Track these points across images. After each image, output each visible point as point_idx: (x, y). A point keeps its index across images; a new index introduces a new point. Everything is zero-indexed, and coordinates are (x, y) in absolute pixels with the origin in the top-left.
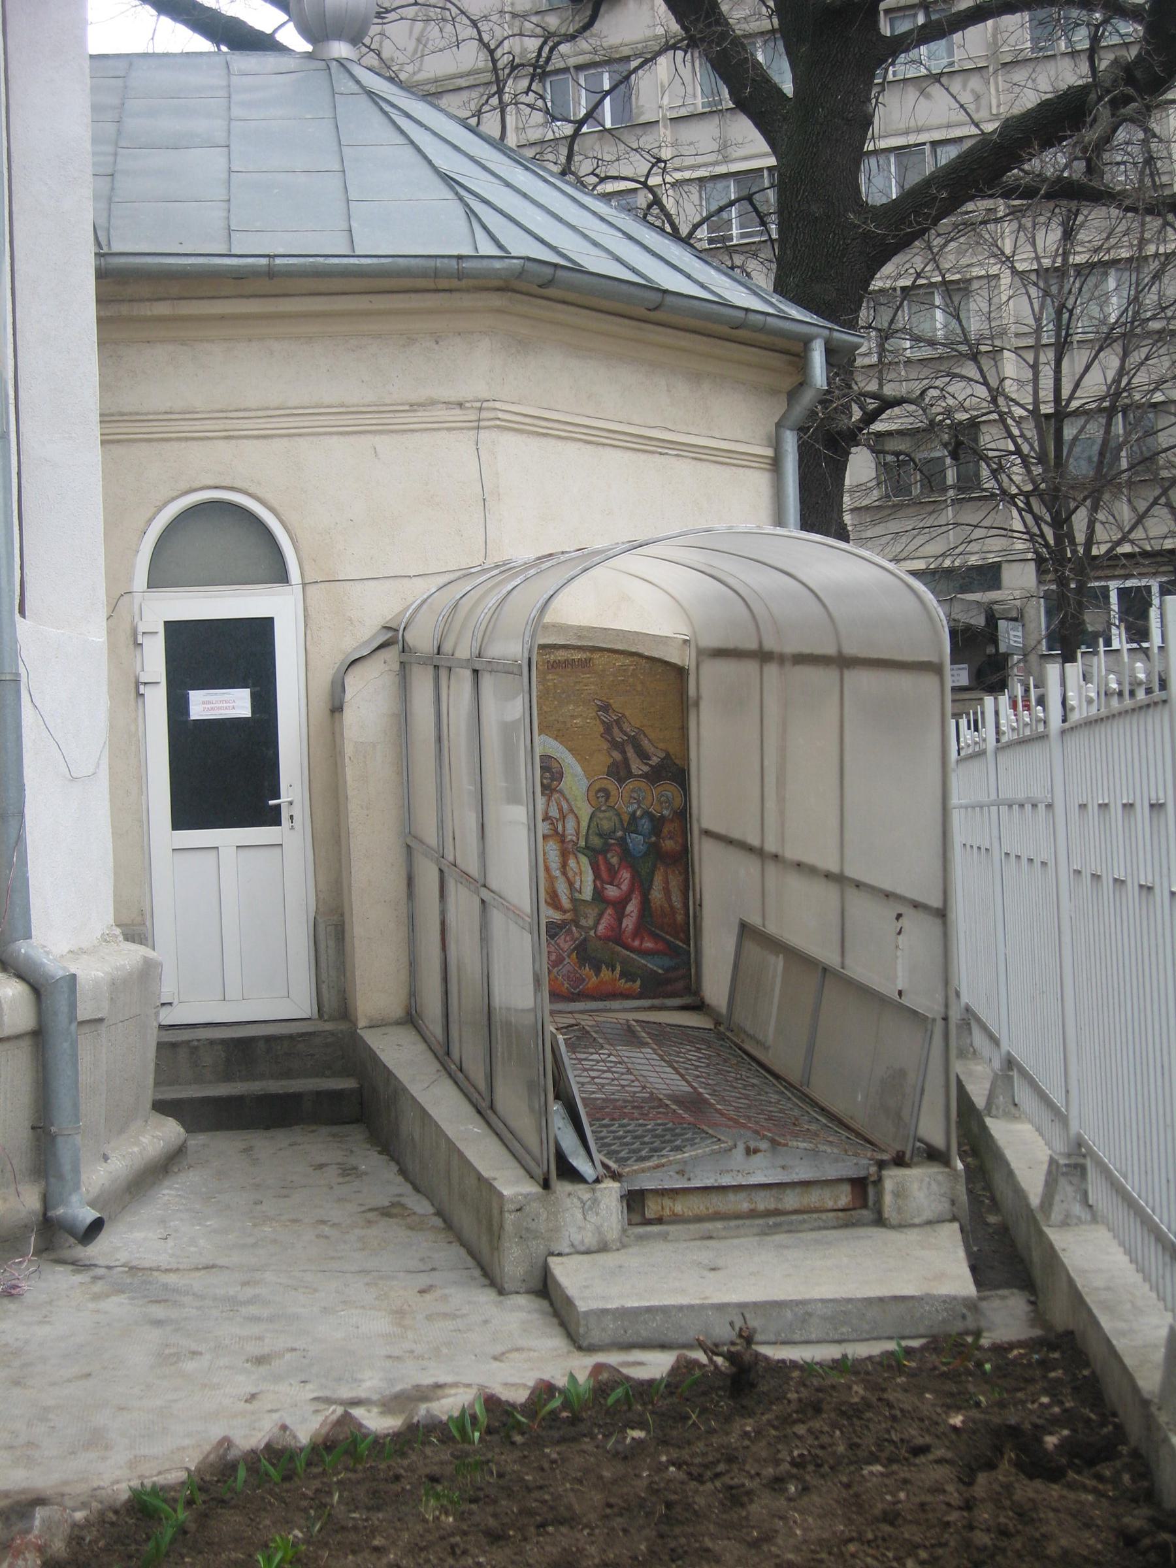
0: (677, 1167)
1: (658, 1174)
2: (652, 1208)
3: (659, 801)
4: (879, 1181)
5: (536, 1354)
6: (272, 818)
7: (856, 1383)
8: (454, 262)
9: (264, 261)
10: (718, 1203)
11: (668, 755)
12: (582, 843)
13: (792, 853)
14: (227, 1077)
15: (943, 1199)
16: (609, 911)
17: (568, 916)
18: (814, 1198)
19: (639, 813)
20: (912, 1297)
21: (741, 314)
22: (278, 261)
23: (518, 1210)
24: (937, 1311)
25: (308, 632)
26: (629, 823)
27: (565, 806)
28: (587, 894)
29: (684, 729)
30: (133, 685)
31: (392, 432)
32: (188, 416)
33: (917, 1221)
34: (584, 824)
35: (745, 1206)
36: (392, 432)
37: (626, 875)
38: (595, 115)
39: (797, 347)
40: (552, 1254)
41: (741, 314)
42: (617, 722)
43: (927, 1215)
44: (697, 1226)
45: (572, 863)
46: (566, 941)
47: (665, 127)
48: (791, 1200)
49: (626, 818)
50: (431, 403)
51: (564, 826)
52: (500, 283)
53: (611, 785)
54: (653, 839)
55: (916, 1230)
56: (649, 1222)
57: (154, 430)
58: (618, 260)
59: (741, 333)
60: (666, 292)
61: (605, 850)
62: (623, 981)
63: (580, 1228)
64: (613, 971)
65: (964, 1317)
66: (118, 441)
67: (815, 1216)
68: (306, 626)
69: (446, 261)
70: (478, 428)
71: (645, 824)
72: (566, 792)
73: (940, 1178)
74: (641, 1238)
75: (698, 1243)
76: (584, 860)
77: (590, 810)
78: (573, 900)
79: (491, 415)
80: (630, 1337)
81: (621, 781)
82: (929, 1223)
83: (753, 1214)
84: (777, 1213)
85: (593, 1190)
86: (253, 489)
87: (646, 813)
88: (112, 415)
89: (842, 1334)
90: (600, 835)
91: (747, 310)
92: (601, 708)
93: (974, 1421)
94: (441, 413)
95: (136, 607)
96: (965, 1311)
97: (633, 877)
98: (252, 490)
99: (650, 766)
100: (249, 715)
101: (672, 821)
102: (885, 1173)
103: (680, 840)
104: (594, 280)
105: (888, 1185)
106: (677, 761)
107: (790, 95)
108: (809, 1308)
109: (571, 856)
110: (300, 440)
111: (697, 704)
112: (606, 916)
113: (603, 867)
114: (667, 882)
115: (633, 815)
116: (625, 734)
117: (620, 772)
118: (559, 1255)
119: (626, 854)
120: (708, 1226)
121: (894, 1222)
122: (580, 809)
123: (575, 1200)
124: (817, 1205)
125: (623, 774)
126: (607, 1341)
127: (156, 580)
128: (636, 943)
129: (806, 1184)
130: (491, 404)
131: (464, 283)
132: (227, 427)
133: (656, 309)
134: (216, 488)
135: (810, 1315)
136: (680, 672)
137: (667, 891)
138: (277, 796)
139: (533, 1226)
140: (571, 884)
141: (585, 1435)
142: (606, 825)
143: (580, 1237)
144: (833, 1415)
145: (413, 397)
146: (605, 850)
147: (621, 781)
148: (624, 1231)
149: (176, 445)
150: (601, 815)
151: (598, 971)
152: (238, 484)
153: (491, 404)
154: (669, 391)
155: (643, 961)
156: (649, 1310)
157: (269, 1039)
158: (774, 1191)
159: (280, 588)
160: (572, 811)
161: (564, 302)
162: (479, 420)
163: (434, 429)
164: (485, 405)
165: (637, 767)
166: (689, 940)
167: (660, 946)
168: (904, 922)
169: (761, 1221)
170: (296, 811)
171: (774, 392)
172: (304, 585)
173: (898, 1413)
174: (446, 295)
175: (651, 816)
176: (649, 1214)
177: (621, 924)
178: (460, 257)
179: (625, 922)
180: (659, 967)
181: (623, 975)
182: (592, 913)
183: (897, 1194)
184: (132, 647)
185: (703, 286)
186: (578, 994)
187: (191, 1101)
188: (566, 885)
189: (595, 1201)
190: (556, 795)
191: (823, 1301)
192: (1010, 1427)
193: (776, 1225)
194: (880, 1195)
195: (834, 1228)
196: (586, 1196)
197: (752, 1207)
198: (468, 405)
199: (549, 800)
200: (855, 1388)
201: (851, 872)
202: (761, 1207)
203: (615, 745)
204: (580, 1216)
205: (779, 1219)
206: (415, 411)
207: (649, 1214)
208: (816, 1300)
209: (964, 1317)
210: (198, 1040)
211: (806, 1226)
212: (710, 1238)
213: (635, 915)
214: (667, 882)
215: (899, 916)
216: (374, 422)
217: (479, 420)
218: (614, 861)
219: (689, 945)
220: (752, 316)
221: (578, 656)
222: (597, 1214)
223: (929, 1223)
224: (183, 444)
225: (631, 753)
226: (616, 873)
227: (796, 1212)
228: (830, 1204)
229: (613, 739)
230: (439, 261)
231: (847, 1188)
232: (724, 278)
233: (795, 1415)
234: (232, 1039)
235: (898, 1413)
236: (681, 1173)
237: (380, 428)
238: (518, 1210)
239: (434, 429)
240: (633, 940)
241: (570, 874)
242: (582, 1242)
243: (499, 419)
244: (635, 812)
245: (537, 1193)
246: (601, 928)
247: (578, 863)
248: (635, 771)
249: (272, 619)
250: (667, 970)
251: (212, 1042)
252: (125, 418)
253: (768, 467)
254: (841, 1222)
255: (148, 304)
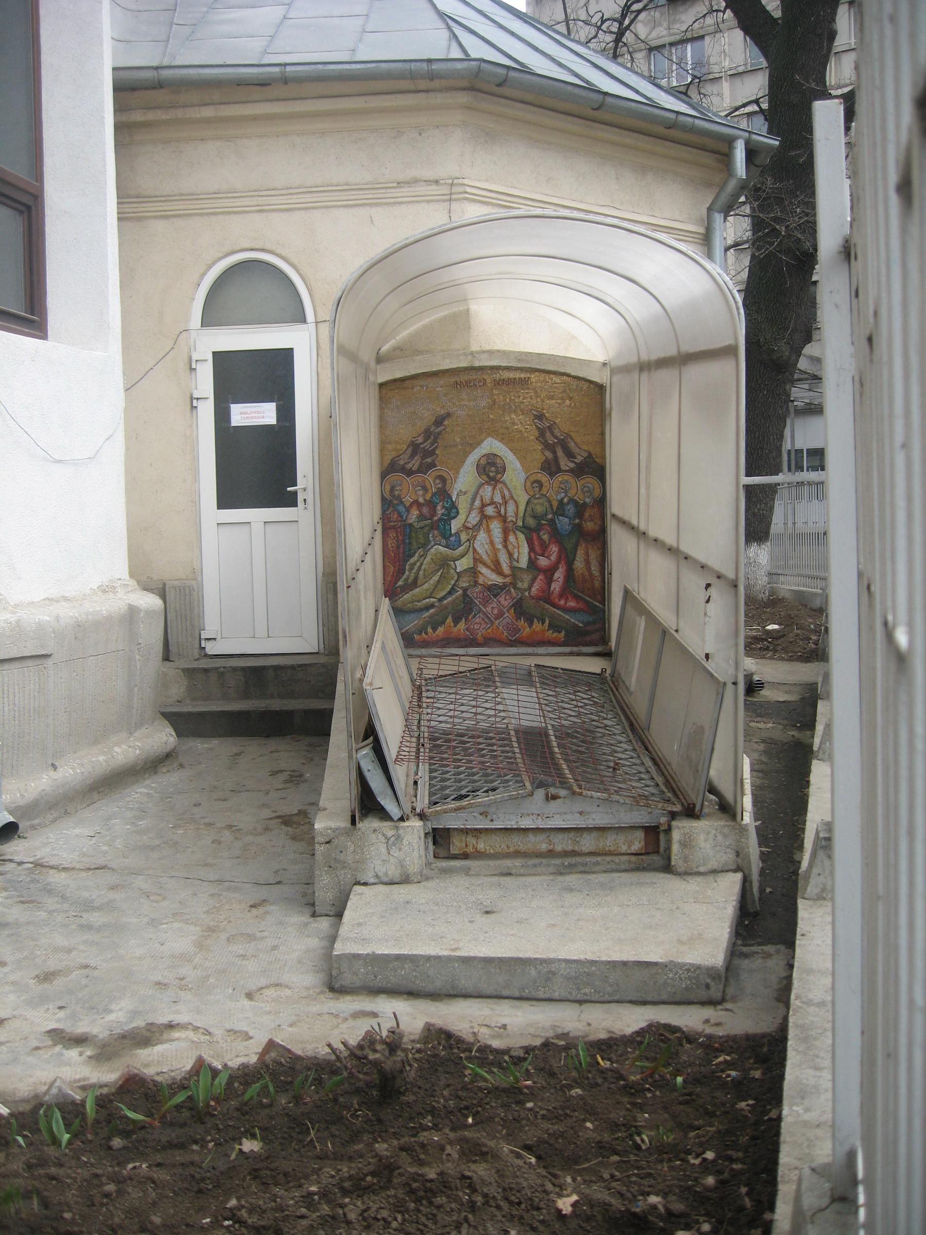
0: (482, 809)
1: (462, 814)
2: (457, 845)
3: (582, 491)
4: (669, 830)
5: (288, 992)
6: (291, 501)
7: (451, 1143)
8: (425, 65)
9: (277, 69)
10: (517, 843)
11: (590, 455)
12: (520, 523)
13: (653, 532)
14: (246, 695)
15: (728, 850)
16: (541, 577)
17: (508, 580)
18: (610, 842)
19: (566, 500)
20: (656, 964)
21: (673, 116)
22: (288, 69)
23: (327, 843)
24: (681, 979)
25: (319, 359)
26: (558, 508)
27: (507, 494)
28: (524, 562)
29: (603, 434)
30: (189, 400)
31: (385, 204)
32: (229, 195)
33: (702, 869)
34: (522, 508)
35: (544, 847)
36: (385, 204)
37: (554, 549)
38: (631, 28)
39: (723, 148)
40: (358, 883)
41: (673, 116)
42: (550, 428)
43: (713, 864)
44: (498, 862)
45: (512, 538)
46: (506, 600)
47: (726, 80)
48: (587, 843)
49: (555, 504)
50: (415, 181)
51: (505, 510)
52: (464, 83)
53: (544, 478)
54: (577, 521)
55: (699, 879)
56: (455, 857)
57: (203, 206)
58: (560, 65)
59: (673, 133)
60: (606, 94)
61: (538, 529)
62: (551, 632)
63: (384, 861)
64: (543, 623)
65: (707, 986)
66: (179, 216)
67: (608, 858)
68: (318, 355)
69: (418, 64)
70: (450, 200)
71: (571, 509)
72: (508, 482)
73: (726, 830)
74: (444, 871)
75: (495, 879)
76: (521, 537)
77: (527, 497)
78: (512, 568)
79: (461, 189)
80: (379, 982)
81: (552, 475)
82: (714, 872)
83: (551, 854)
84: (574, 853)
85: (397, 828)
86: (279, 250)
87: (572, 500)
88: (175, 195)
89: (585, 994)
90: (534, 517)
91: (678, 113)
92: (536, 417)
93: (591, 1204)
94: (422, 189)
95: (192, 340)
96: (708, 981)
97: (560, 551)
98: (279, 251)
99: (575, 463)
100: (275, 423)
101: (593, 506)
102: (674, 823)
103: (599, 522)
104: (544, 81)
105: (676, 835)
106: (597, 460)
107: (778, 14)
108: (554, 967)
109: (511, 533)
110: (315, 211)
111: (610, 414)
112: (538, 581)
113: (536, 543)
114: (587, 554)
115: (561, 502)
116: (556, 438)
117: (551, 468)
118: (365, 884)
119: (556, 534)
120: (508, 863)
121: (679, 870)
122: (518, 496)
123: (380, 836)
124: (611, 849)
125: (553, 468)
126: (358, 984)
127: (210, 318)
128: (562, 602)
129: (602, 829)
130: (460, 181)
131: (436, 83)
132: (260, 203)
133: (597, 109)
134: (252, 250)
135: (554, 974)
136: (601, 388)
137: (587, 563)
138: (294, 484)
139: (341, 857)
140: (510, 555)
141: (196, 1142)
142: (539, 510)
143: (384, 870)
144: (401, 1193)
145: (401, 177)
146: (538, 529)
147: (552, 475)
148: (428, 864)
149: (221, 217)
150: (536, 501)
151: (531, 624)
152: (268, 246)
153: (460, 181)
154: (617, 179)
155: (567, 617)
156: (398, 958)
157: (276, 668)
158: (572, 834)
159: (304, 326)
160: (512, 498)
161: (522, 102)
162: (451, 194)
163: (417, 202)
164: (456, 181)
165: (565, 464)
166: (604, 602)
167: (581, 605)
168: (713, 591)
169: (558, 861)
170: (309, 496)
171: (708, 185)
172: (317, 323)
173: (479, 1199)
174: (424, 95)
175: (576, 503)
176: (454, 850)
177: (550, 587)
178: (429, 61)
179: (553, 586)
180: (580, 622)
181: (551, 626)
182: (527, 578)
183: (684, 844)
184: (188, 371)
185: (637, 92)
186: (515, 641)
187: (211, 714)
188: (507, 556)
189: (398, 838)
190: (499, 486)
191: (566, 961)
192: (635, 1215)
193: (571, 866)
194: (669, 842)
195: (626, 871)
196: (390, 833)
197: (551, 847)
198: (442, 182)
199: (494, 489)
200: (449, 1149)
201: (684, 548)
202: (559, 848)
203: (547, 446)
204: (384, 850)
205: (573, 860)
206: (402, 187)
207: (454, 850)
208: (560, 960)
209: (707, 986)
210: (224, 667)
211: (598, 868)
212: (510, 874)
213: (561, 580)
214: (587, 554)
215: (708, 586)
216: (371, 196)
217: (451, 194)
218: (545, 537)
219: (604, 605)
220: (681, 118)
221: (518, 375)
222: (400, 850)
223: (714, 872)
224: (227, 217)
225: (560, 453)
226: (547, 547)
227: (591, 854)
228: (624, 849)
229: (546, 441)
230: (413, 64)
231: (640, 834)
232: (670, 97)
233: (369, 1178)
234: (249, 668)
235: (479, 1199)
236: (484, 814)
237: (375, 201)
238: (327, 843)
239: (417, 202)
240: (559, 600)
241: (510, 547)
242: (386, 874)
243: (466, 192)
244: (562, 499)
245: (345, 828)
246: (534, 590)
247: (517, 539)
248: (563, 467)
249: (292, 349)
250: (587, 624)
251: (234, 669)
252: (183, 197)
253: (699, 241)
254: (633, 866)
255: (197, 108)
